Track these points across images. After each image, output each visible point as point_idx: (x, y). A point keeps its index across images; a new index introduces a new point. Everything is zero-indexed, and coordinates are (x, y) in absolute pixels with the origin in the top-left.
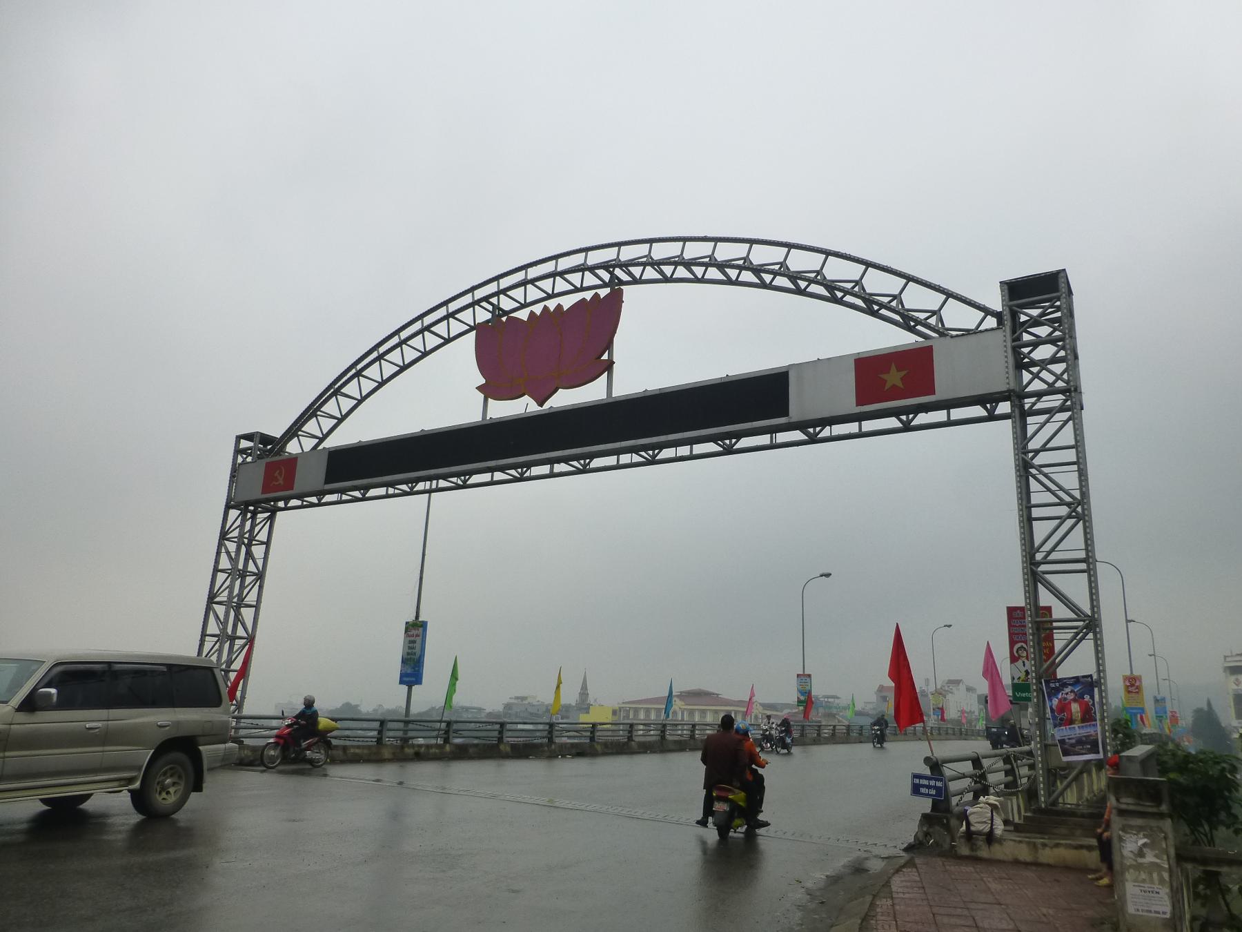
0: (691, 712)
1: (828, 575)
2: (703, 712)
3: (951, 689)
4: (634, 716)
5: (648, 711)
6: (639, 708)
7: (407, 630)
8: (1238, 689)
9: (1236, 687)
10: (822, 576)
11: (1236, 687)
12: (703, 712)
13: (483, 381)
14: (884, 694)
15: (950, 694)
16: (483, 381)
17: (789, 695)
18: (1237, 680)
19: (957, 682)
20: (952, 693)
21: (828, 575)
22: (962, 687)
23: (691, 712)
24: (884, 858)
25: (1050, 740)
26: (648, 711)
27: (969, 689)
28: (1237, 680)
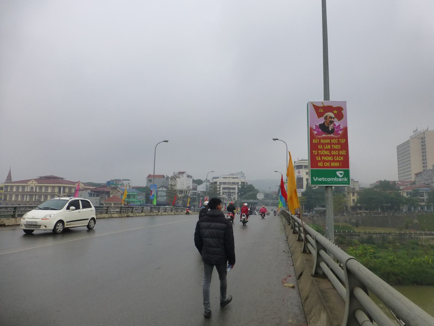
0: (41, 187)
1: (167, 141)
2: (47, 187)
3: (180, 176)
4: (11, 190)
5: (18, 187)
6: (19, 186)
7: (398, 149)
8: (299, 176)
9: (298, 175)
10: (164, 141)
11: (298, 175)
12: (47, 187)
13: (342, 111)
14: (150, 179)
15: (178, 178)
16: (342, 111)
17: (28, 183)
18: (299, 171)
19: (182, 173)
20: (179, 178)
21: (167, 141)
22: (185, 175)
23: (41, 187)
24: (362, 323)
25: (123, 209)
26: (18, 187)
27: (188, 176)
28: (299, 171)
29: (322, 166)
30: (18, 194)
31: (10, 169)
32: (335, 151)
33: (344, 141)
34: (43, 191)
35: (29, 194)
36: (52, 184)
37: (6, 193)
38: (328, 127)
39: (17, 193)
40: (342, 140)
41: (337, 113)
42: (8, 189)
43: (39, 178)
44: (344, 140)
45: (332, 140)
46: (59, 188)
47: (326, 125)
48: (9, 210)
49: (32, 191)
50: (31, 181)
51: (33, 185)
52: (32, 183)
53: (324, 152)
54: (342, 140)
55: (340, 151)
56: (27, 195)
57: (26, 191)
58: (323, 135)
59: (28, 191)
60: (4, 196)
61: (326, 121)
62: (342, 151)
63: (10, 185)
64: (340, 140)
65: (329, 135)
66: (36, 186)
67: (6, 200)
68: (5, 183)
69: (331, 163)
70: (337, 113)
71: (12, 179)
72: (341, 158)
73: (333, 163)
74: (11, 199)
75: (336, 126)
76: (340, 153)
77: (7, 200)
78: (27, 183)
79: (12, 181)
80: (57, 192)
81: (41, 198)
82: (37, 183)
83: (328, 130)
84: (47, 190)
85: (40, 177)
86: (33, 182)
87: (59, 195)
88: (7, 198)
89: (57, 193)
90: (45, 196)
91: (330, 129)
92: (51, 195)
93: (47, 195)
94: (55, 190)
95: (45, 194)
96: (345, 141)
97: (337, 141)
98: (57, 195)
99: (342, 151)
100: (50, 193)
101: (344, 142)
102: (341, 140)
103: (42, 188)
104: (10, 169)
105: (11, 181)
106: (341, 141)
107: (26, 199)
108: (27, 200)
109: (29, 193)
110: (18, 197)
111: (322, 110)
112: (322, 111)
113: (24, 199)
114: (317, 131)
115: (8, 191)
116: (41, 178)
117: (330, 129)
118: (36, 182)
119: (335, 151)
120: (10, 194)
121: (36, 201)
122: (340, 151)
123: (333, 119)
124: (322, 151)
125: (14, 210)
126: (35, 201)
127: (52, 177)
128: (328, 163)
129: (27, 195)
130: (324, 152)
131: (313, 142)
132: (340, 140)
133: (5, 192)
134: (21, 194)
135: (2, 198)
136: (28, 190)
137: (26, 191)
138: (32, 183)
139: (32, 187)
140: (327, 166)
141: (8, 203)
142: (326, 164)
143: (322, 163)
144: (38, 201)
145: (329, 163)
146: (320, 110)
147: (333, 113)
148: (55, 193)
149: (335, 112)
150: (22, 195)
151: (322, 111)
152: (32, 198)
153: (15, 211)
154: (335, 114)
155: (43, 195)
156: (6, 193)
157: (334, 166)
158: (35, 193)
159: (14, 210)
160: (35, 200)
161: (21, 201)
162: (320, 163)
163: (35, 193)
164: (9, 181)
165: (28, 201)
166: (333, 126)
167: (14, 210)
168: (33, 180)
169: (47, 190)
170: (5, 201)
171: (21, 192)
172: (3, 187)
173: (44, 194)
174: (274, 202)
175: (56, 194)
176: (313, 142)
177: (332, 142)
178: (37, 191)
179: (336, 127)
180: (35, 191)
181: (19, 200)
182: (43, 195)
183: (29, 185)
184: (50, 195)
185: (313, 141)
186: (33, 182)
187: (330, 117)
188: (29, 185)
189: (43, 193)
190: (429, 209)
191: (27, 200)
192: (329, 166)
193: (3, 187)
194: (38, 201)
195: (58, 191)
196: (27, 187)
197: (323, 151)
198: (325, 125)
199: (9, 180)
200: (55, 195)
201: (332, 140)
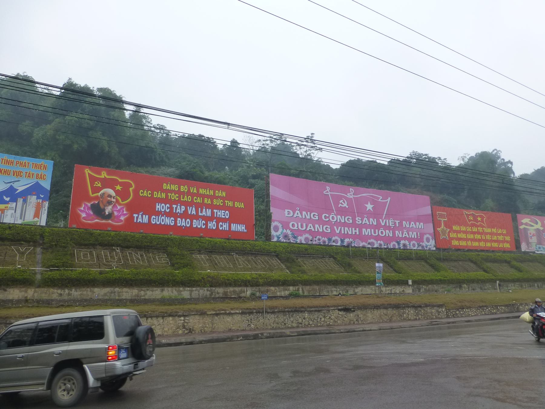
29: (214, 228)
32: (184, 220)
33: (183, 210)
38: (104, 210)
40: (179, 207)
41: (120, 190)
44: (183, 207)
45: (158, 205)
47: (101, 206)
53: (163, 219)
54: (179, 207)
55: (194, 221)
58: (95, 220)
61: (102, 201)
62: (198, 221)
64: (174, 206)
65: (104, 221)
69: (232, 224)
70: (120, 190)
72: (224, 226)
73: (234, 224)
75: (117, 208)
76: (194, 223)
83: (103, 213)
91: (107, 213)
96: (184, 210)
97: (168, 208)
99: (198, 221)
101: (182, 212)
102: (177, 207)
106: (176, 208)
111: (100, 184)
112: (99, 185)
114: (87, 214)
117: (107, 213)
119: (184, 220)
122: (194, 221)
123: (112, 198)
124: (160, 217)
128: (226, 223)
130: (163, 219)
131: (164, 188)
132: (174, 206)
140: (224, 229)
142: (222, 226)
143: (214, 223)
145: (228, 224)
146: (96, 183)
147: (114, 189)
149: (118, 188)
151: (99, 185)
154: (117, 192)
157: (236, 230)
162: (211, 222)
166: (111, 209)
176: (164, 188)
177: (158, 208)
179: (117, 209)
185: (164, 186)
187: (109, 195)
192: (228, 229)
197: (163, 218)
198: (100, 207)
201: (158, 205)
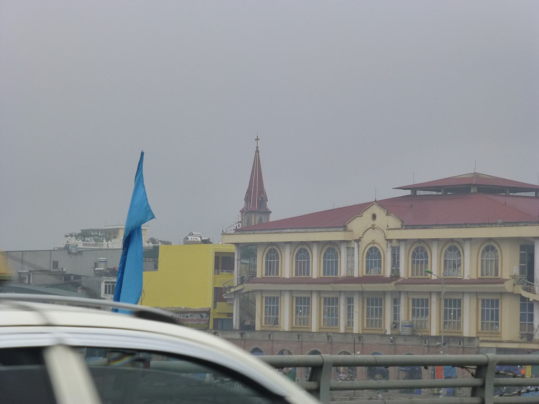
30: (334, 292)
31: (257, 151)
34: (435, 270)
35: (362, 293)
36: (481, 225)
37: (248, 287)
39: (328, 288)
42: (255, 267)
43: (408, 192)
46: (522, 248)
48: (392, 382)
49: (373, 273)
50: (367, 214)
51: (377, 237)
52: (373, 227)
56: (350, 301)
57: (343, 272)
59: (356, 275)
60: (241, 308)
63: (318, 243)
66: (395, 244)
67: (251, 328)
68: (238, 231)
71: (270, 205)
74: (276, 322)
77: (258, 327)
78: (345, 228)
79: (273, 218)
80: (514, 277)
81: (426, 313)
82: (398, 224)
84: (457, 265)
85: (414, 188)
86: (374, 217)
87: (525, 294)
88: (253, 317)
89: (512, 282)
90: (446, 300)
92: (481, 297)
93: (457, 297)
94: (497, 261)
95: (447, 293)
98: (512, 294)
100: (471, 282)
103: (427, 257)
104: (257, 151)
105: (264, 220)
107: (349, 323)
108: (356, 329)
109: (357, 287)
110: (308, 311)
113: (337, 322)
115: (255, 274)
116: (420, 193)
118: (393, 222)
120: (327, 296)
121: (399, 335)
125: (311, 380)
126: (396, 336)
127: (474, 182)
129: (350, 301)
133: (242, 280)
134: (319, 292)
135: (231, 315)
136: (352, 270)
137: (343, 272)
138: (373, 227)
139: (371, 249)
141: (260, 348)
144: (413, 335)
148: (502, 281)
150: (328, 301)
152: (380, 312)
153: (483, 386)
155: (434, 300)
156: (248, 287)
158: (390, 287)
159: (311, 380)
160: (395, 326)
161: (325, 335)
163: (390, 287)
164: (255, 220)
165: (360, 337)
167: (477, 382)
168: (376, 209)
169: (454, 266)
170: (248, 335)
171: (319, 281)
172: (233, 253)
173: (439, 293)
174: (484, 266)
175: (508, 287)
178: (403, 274)
180: (388, 274)
181: (314, 328)
182: (434, 300)
183: (358, 241)
184: (477, 293)
186: (374, 217)
188: (358, 241)
189: (437, 282)
190: (492, 275)
191: (356, 329)
193: (233, 253)
194: (413, 335)
195: (516, 270)
196: (350, 250)
199: (255, 212)
200: (502, 294)
